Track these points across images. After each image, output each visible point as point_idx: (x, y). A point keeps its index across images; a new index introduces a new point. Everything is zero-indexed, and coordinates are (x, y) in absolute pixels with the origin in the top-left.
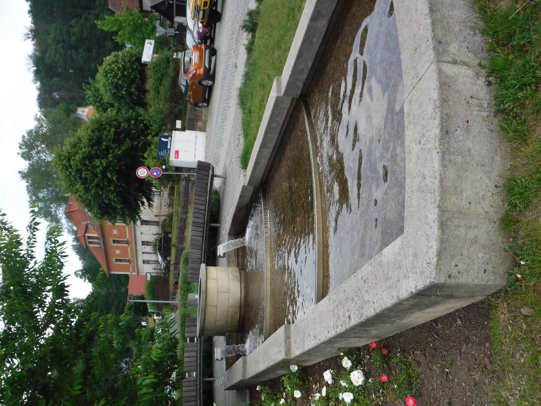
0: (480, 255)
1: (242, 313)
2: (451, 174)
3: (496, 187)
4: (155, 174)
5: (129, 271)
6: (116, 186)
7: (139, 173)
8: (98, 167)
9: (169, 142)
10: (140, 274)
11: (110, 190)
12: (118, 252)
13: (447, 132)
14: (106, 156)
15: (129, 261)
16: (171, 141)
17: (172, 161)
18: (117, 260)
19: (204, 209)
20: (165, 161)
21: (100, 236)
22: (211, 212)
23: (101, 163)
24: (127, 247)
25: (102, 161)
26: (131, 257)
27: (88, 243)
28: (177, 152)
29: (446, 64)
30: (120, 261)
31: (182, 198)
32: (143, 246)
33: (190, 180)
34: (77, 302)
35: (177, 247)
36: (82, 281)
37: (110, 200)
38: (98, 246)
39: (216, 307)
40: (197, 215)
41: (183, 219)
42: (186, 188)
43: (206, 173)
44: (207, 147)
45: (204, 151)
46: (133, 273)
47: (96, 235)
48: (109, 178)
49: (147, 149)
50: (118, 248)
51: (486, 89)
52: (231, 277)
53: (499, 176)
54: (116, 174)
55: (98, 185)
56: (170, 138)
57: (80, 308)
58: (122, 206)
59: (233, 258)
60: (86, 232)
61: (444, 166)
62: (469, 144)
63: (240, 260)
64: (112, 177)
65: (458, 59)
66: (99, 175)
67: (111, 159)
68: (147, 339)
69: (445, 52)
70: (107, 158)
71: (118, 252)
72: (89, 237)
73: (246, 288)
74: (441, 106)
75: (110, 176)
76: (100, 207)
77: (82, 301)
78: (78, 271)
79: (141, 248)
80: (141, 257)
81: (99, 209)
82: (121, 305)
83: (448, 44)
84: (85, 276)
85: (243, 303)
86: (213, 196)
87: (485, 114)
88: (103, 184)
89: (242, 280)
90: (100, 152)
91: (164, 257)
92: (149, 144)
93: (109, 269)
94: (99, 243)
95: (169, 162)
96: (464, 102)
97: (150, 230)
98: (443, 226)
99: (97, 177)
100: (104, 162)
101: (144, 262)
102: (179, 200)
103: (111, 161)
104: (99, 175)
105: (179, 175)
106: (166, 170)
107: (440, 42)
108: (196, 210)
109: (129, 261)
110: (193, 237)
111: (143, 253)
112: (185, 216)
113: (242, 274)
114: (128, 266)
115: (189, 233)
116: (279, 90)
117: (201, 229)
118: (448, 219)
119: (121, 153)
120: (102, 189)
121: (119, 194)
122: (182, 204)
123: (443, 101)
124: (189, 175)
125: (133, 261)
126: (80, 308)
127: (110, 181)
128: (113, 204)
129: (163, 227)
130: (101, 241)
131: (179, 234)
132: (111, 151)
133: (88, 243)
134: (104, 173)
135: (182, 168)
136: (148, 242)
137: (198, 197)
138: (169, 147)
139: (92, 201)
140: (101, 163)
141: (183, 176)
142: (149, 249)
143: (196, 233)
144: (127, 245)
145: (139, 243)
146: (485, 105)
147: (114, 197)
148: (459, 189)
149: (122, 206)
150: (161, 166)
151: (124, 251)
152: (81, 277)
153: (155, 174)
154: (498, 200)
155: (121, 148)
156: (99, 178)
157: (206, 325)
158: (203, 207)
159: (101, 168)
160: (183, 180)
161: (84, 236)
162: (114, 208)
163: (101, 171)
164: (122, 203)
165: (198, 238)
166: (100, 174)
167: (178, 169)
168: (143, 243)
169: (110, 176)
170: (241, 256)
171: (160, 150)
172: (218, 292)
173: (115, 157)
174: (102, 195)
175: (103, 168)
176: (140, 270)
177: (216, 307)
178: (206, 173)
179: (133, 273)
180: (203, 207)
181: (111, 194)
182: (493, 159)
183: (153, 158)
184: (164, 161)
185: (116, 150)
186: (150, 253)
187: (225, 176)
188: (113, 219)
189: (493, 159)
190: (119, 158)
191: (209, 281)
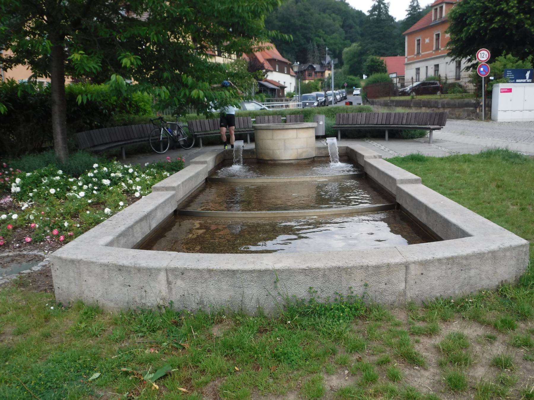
0: (64, 285)
1: (270, 162)
2: (98, 270)
3: (97, 301)
4: (482, 69)
5: (408, 55)
6: (485, 29)
7: (482, 52)
8: (507, 4)
9: (524, 81)
10: (406, 67)
11: (481, 23)
12: (427, 41)
13: (120, 270)
14: (521, 10)
15: (418, 53)
16: (526, 82)
17: (498, 86)
18: (419, 40)
19: (391, 123)
20: (500, 78)
21: (443, 20)
22: (401, 131)
23: (513, 7)
24: (432, 49)
25: (514, 9)
26: (422, 55)
27: (436, 7)
28: (510, 90)
29: (165, 275)
30: (419, 44)
31: (457, 101)
32: (433, 67)
33: (476, 108)
34: (385, 6)
35: (411, 101)
36: (407, 8)
37: (470, 24)
38: (433, 19)
39: (272, 139)
40: (397, 117)
41: (438, 105)
42: (468, 105)
43: (436, 122)
44: (517, 123)
45: (512, 121)
46: (406, 60)
47: (444, 14)
48: (494, 20)
49: (516, 57)
50: (431, 40)
51: (155, 303)
52: (300, 151)
53: (103, 304)
54: (499, 26)
55: (486, 8)
56: (530, 80)
57: (380, 11)
58: (464, 39)
59: (324, 152)
60: (447, 3)
61: (101, 265)
62: (116, 285)
63: (323, 159)
64: (496, 22)
65: (172, 286)
66: (498, 8)
67: (517, 17)
68: (349, 81)
69: (176, 277)
70: (518, 14)
71: (427, 41)
72: (442, 7)
73: (291, 164)
74: (135, 268)
75: (496, 20)
76: (462, 15)
77: (387, 11)
78: (418, 2)
79: (431, 64)
80: (422, 66)
81: (460, 15)
82: (382, 51)
83: (183, 279)
84: (412, 10)
85: (277, 162)
86: (418, 131)
87: (137, 299)
88: (488, 14)
89: (298, 161)
90: (527, 4)
91: (414, 90)
92: (523, 59)
93: (409, 34)
94: (435, 19)
95: (498, 82)
96: (142, 285)
97: (451, 72)
98: (72, 261)
99: (495, 6)
100: (514, 10)
101: (418, 69)
102: (456, 98)
103: (515, 18)
104: (498, 8)
105: (481, 96)
106: (487, 80)
107: (183, 274)
108: (402, 115)
109: (418, 53)
110: (377, 115)
111: (427, 67)
112: (440, 106)
113: (306, 161)
114: (413, 54)
115: (400, 110)
116: (403, 182)
117: (384, 122)
118: (76, 265)
119: (526, 28)
120: (482, 14)
121: (477, 32)
122: (452, 102)
123: (139, 270)
124: (482, 106)
125: (419, 58)
126: (380, 11)
127: (491, 21)
128: (465, 29)
129: (453, 85)
130: (438, 21)
131: (424, 102)
132: (528, 16)
133: (436, 7)
134: (501, 12)
135: (491, 98)
136: (438, 70)
137: (414, 115)
138: (517, 81)
139: (468, 5)
140: (513, 7)
141: (480, 100)
142: (431, 73)
143: (380, 117)
144: (434, 49)
145: (436, 62)
146: (143, 301)
147: (473, 28)
148: (91, 274)
149: (464, 39)
150: (492, 74)
151: (428, 47)
152: (411, 6)
153: (482, 69)
154: (91, 301)
155: (532, 27)
156: (494, 8)
157: (259, 131)
158: (404, 121)
159: (505, 9)
160: (476, 100)
161: (442, 3)
162: (461, 31)
163: (503, 8)
164: (467, 38)
165: (376, 119)
166: (499, 10)
167: (489, 94)
168: (437, 66)
169: (496, 20)
170: (321, 159)
171: (514, 72)
172: (285, 140)
173: (521, 21)
174: (475, 15)
175: (506, 11)
176: (410, 66)
177: (272, 139)
178: (436, 122)
179: (406, 60)
180: (404, 121)
181: (476, 24)
182: (112, 301)
183: (505, 65)
184: (499, 77)
185: (529, 22)
186: (427, 74)
187: (431, 142)
188: (452, 31)
189: (112, 301)
190: (520, 25)
191: (295, 131)
